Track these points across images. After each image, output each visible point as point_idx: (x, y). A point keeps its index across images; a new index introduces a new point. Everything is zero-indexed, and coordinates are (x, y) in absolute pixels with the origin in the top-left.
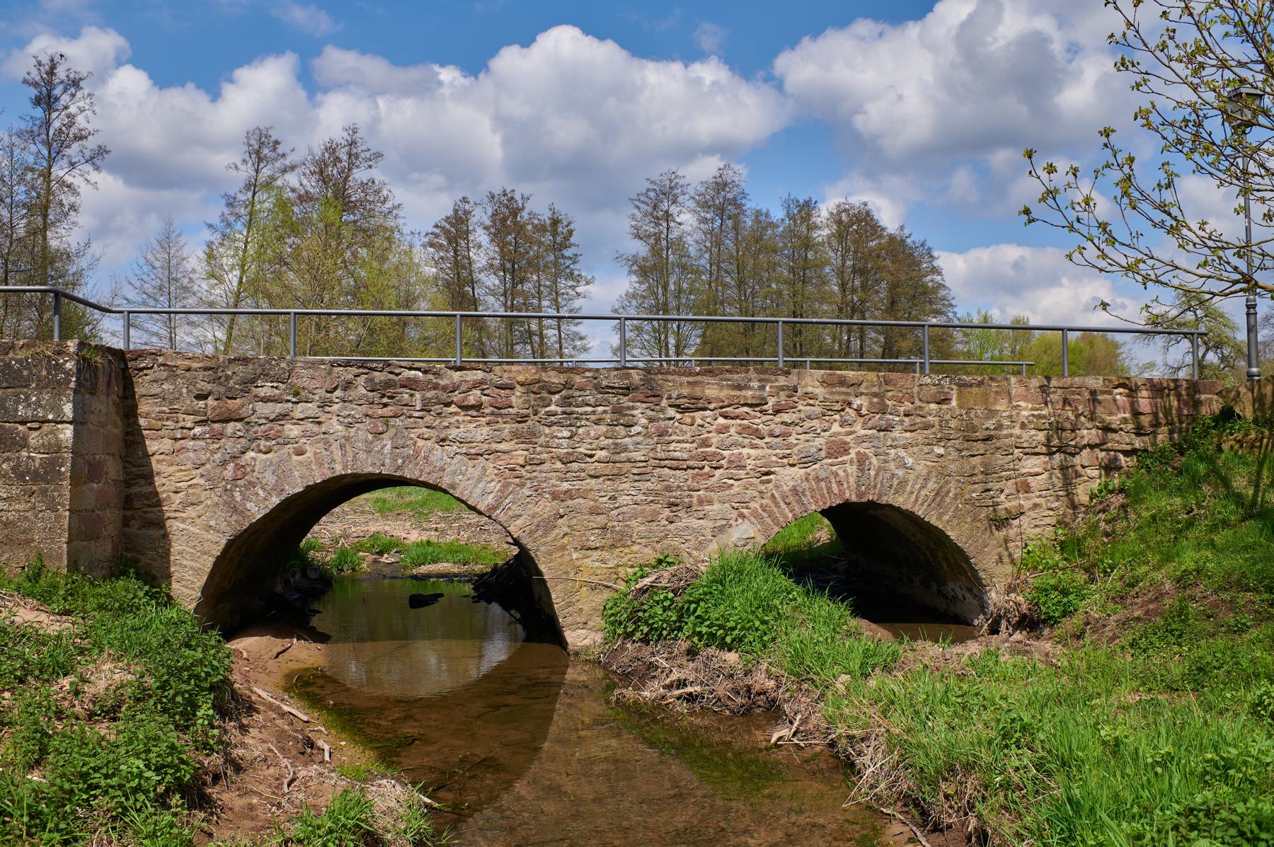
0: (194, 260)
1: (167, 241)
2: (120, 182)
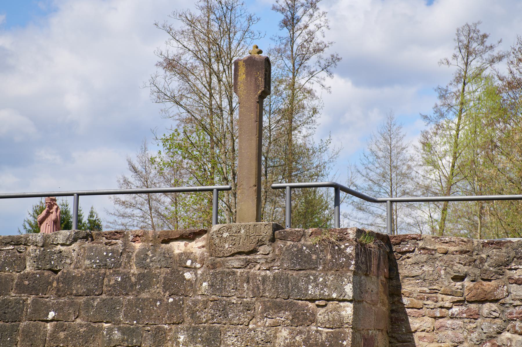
0: (412, 147)
1: (389, 134)
2: (349, 84)
